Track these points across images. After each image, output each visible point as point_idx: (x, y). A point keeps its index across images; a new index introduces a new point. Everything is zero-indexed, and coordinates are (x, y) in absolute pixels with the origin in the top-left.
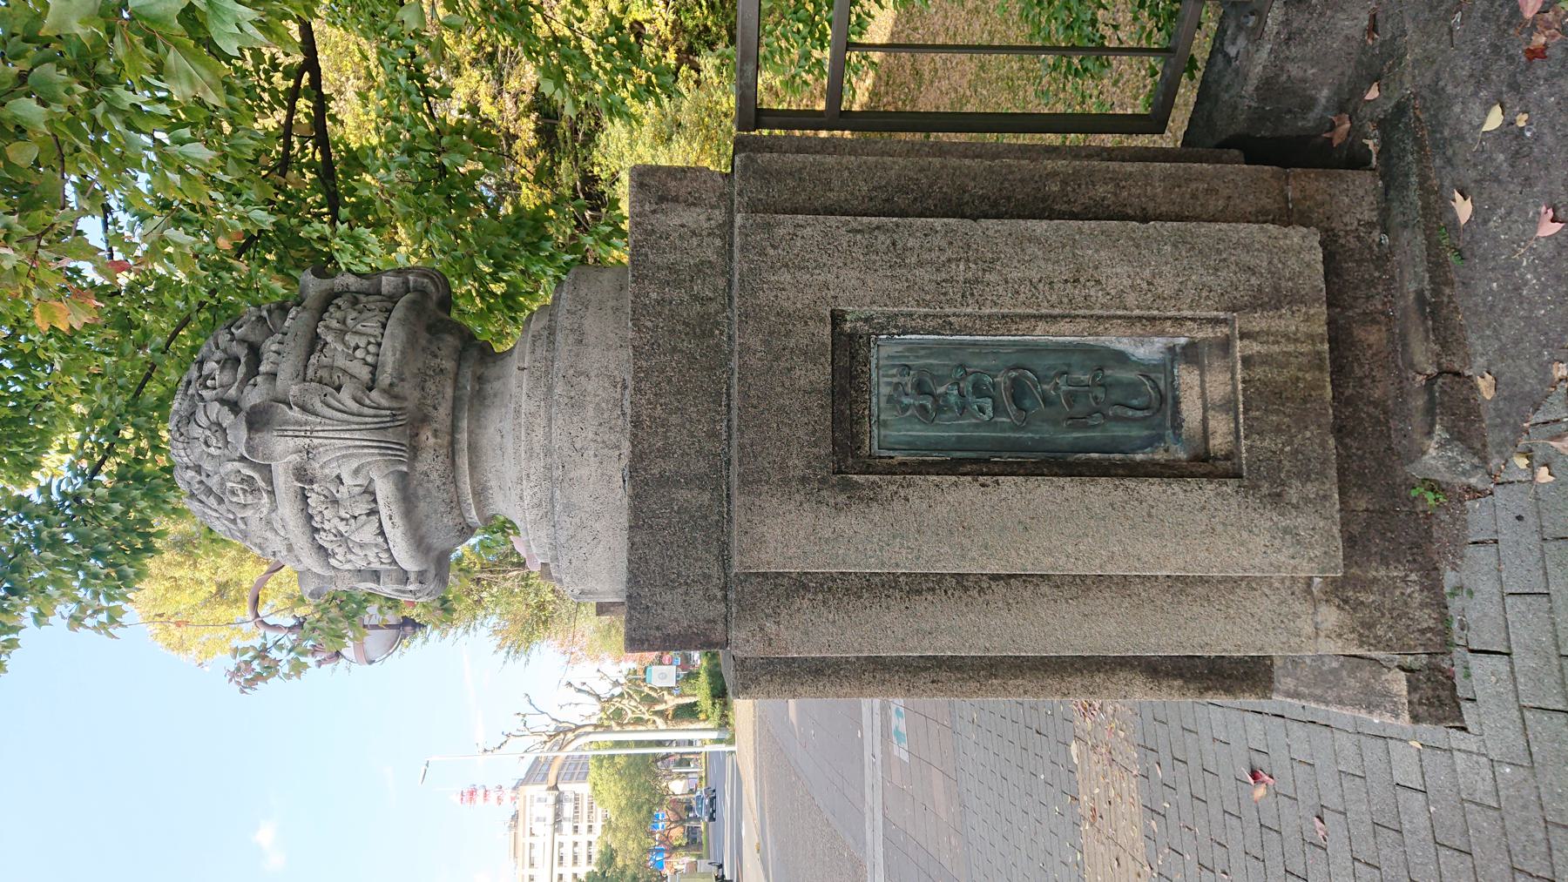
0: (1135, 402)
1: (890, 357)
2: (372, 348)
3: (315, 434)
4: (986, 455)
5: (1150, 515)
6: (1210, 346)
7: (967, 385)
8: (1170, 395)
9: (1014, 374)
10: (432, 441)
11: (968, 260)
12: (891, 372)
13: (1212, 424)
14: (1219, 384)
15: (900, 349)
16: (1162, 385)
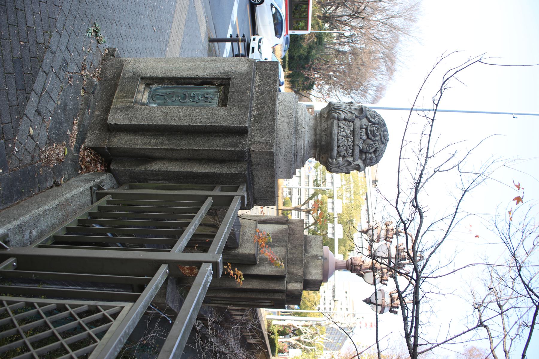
0: (158, 96)
2: (340, 131)
4: (195, 86)
6: (139, 104)
7: (196, 99)
8: (150, 97)
9: (185, 101)
10: (325, 115)
11: (192, 116)
13: (143, 90)
14: (140, 96)
16: (151, 99)
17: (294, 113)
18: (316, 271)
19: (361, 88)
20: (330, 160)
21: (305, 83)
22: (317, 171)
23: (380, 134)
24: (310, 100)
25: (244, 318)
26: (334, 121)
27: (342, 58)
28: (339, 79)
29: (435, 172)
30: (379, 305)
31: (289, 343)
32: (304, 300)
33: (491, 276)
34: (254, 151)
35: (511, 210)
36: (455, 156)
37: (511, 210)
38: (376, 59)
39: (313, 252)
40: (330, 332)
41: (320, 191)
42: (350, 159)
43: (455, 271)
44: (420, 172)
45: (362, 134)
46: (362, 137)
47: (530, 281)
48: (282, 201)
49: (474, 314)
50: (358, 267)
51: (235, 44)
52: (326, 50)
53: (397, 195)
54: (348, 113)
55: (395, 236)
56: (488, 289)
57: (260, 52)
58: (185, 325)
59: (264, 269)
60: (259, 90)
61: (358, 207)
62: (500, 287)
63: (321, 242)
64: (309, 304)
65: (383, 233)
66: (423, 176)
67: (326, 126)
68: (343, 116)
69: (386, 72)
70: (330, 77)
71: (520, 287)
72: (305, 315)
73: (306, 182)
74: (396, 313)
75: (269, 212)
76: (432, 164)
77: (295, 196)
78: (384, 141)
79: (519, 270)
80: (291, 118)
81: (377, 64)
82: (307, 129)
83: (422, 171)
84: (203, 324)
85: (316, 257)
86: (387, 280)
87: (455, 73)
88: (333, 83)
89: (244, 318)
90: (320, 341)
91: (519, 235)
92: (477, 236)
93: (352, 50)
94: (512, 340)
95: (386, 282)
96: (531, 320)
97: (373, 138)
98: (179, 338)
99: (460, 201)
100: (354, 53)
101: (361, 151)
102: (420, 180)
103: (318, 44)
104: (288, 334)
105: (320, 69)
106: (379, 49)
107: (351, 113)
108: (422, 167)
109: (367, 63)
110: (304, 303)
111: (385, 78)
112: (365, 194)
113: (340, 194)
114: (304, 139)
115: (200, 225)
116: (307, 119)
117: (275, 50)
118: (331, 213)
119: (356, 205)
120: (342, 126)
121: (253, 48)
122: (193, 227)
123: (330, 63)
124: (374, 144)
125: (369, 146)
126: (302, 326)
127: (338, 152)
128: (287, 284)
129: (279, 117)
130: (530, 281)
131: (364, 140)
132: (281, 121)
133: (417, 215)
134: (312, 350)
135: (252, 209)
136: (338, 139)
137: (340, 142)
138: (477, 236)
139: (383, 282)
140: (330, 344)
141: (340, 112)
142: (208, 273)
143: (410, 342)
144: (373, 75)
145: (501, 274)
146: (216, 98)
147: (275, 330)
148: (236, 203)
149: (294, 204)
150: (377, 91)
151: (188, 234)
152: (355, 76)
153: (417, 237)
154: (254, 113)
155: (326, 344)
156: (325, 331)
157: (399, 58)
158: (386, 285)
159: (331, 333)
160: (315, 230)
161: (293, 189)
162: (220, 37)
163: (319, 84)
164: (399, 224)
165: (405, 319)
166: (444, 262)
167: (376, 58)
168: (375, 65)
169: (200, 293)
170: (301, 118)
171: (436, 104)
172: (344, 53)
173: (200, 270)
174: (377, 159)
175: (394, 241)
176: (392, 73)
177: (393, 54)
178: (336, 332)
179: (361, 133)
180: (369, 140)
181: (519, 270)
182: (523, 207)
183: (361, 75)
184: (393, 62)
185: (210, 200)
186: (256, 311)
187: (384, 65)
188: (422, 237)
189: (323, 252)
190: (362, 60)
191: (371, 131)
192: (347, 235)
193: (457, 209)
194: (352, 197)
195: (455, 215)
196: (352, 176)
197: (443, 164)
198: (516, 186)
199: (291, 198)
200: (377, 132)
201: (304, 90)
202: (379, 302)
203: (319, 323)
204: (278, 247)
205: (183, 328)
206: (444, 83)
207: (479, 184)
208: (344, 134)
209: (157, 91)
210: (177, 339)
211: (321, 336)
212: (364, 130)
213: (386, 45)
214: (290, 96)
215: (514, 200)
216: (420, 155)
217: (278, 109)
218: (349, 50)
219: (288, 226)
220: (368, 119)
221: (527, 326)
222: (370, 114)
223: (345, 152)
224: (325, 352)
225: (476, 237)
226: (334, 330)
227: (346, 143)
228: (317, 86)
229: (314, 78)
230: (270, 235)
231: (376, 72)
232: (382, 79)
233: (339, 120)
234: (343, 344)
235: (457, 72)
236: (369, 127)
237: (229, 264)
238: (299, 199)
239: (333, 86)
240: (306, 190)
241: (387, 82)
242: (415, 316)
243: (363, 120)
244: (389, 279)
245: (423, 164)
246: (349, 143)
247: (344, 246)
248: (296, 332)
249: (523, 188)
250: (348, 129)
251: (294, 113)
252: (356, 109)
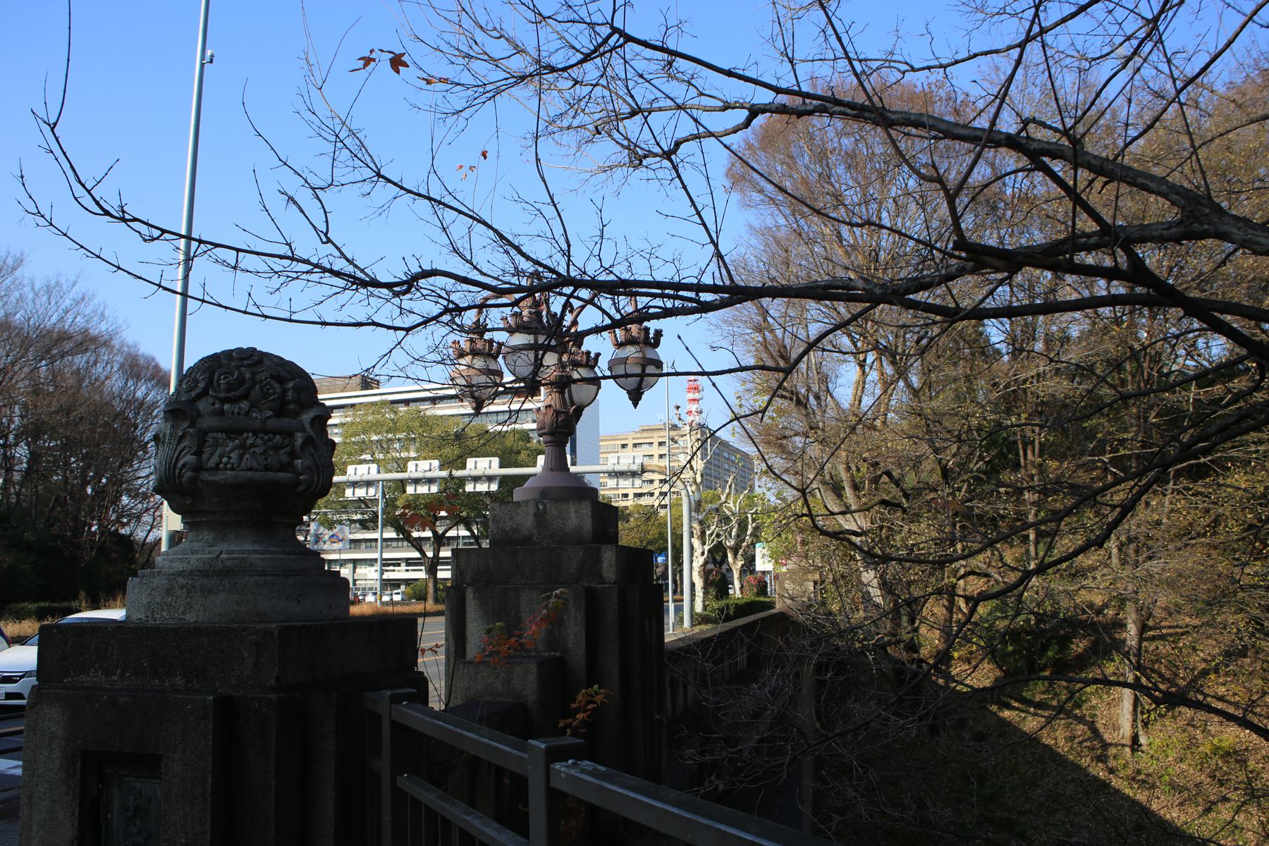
2: (229, 466)
17: (181, 581)
18: (573, 515)
19: (131, 415)
20: (301, 488)
21: (114, 555)
22: (340, 522)
23: (238, 368)
24: (158, 542)
25: (691, 678)
26: (202, 481)
27: (48, 462)
28: (106, 471)
29: (329, 241)
30: (644, 370)
31: (743, 572)
32: (644, 544)
33: (569, 128)
34: (277, 678)
35: (424, 79)
36: (291, 194)
37: (424, 79)
38: (54, 377)
39: (529, 523)
40: (713, 479)
41: (388, 513)
42: (299, 439)
43: (553, 202)
44: (327, 274)
45: (236, 410)
46: (243, 412)
47: (578, 51)
48: (416, 603)
49: (653, 167)
50: (560, 419)
52: (24, 505)
53: (333, 321)
54: (182, 445)
55: (487, 336)
56: (598, 136)
57: (21, 677)
58: (694, 817)
59: (571, 639)
60: (118, 671)
61: (426, 422)
62: (592, 111)
63: (503, 506)
64: (653, 532)
65: (479, 363)
66: (336, 268)
67: (216, 499)
68: (189, 458)
69: (89, 354)
70: (100, 493)
71: (591, 71)
72: (678, 538)
73: (366, 547)
74: (659, 334)
75: (433, 633)
76: (308, 246)
77: (400, 573)
78: (250, 359)
79: (553, 69)
80: (194, 587)
81: (68, 375)
82: (223, 547)
83: (324, 270)
84: (710, 775)
85: (540, 517)
86: (588, 353)
87: (83, 186)
88: (115, 484)
89: (691, 678)
90: (735, 503)
91: (478, 66)
92: (484, 155)
93: (27, 439)
94: (702, 94)
95: (592, 355)
96: (659, 55)
97: (246, 386)
98: (723, 827)
99: (402, 188)
100: (33, 432)
101: (280, 412)
102: (345, 275)
103: (7, 526)
104: (723, 576)
105: (76, 519)
106: (26, 370)
107: (182, 438)
108: (316, 270)
109: (63, 400)
110: (650, 542)
111: (106, 358)
112: (396, 405)
113: (395, 465)
114: (249, 552)
115: (472, 804)
116: (196, 546)
117: (19, 637)
118: (440, 485)
119: (421, 426)
120: (215, 459)
121: (9, 696)
122: (469, 818)
123: (62, 494)
124: (261, 381)
125: (265, 395)
126: (704, 544)
127: (282, 468)
128: (604, 583)
129: (190, 617)
130: (578, 51)
131: (252, 406)
132: (201, 613)
133: (422, 282)
134: (754, 520)
135: (426, 675)
136: (247, 470)
137: (255, 464)
138: (484, 155)
139: (592, 363)
140: (740, 479)
141: (179, 465)
142: (572, 772)
143: (718, 302)
144: (97, 385)
145: (564, 106)
146: (138, 785)
147: (716, 606)
148: (409, 714)
149: (421, 574)
150: (138, 378)
151: (488, 830)
152: (99, 430)
153: (484, 286)
154: (179, 681)
155: (740, 489)
156: (711, 491)
157: (54, 319)
158: (598, 355)
159: (716, 478)
160: (482, 523)
161: (385, 576)
163: (118, 520)
164: (458, 325)
165: (667, 313)
166: (540, 225)
167: (50, 377)
168: (71, 382)
169: (620, 786)
170: (194, 561)
171: (160, 232)
172: (34, 457)
173: (568, 791)
174: (299, 377)
175: (501, 337)
176: (94, 339)
177: (41, 336)
178: (713, 467)
179: (233, 413)
180: (253, 393)
181: (553, 69)
182: (415, 53)
183: (97, 417)
184: (64, 336)
185: (404, 780)
186: (672, 652)
187: (70, 358)
188: (485, 275)
189: (527, 502)
190: (55, 412)
191: (228, 391)
192: (487, 444)
193: (419, 195)
194: (401, 436)
195: (435, 201)
196: (352, 436)
197: (311, 223)
198: (365, 66)
199: (407, 582)
200: (233, 375)
201: (134, 556)
202: (638, 370)
203: (693, 506)
204: (519, 607)
205: (701, 820)
206: (107, 213)
207: (363, 146)
208: (234, 455)
210: (725, 833)
211: (723, 498)
212: (226, 407)
213: (15, 353)
214: (136, 590)
215: (398, 72)
216: (290, 274)
217: (169, 622)
218: (26, 445)
219: (468, 585)
220: (199, 397)
221: (670, 63)
222: (186, 392)
223: (282, 452)
224: (758, 491)
225: (485, 158)
226: (708, 472)
227: (259, 450)
228: (124, 525)
229: (102, 534)
230: (486, 627)
231: (90, 378)
232: (107, 363)
233: (198, 468)
234: (738, 451)
235: (80, 182)
236: (219, 395)
237: (561, 724)
238: (409, 562)
239: (124, 486)
240: (388, 546)
241: (116, 352)
242: (660, 291)
243: (201, 408)
244: (584, 348)
245: (308, 267)
246: (259, 441)
247: (519, 453)
248: (718, 558)
249: (372, 51)
250: (223, 445)
251: (181, 581)
252: (173, 426)
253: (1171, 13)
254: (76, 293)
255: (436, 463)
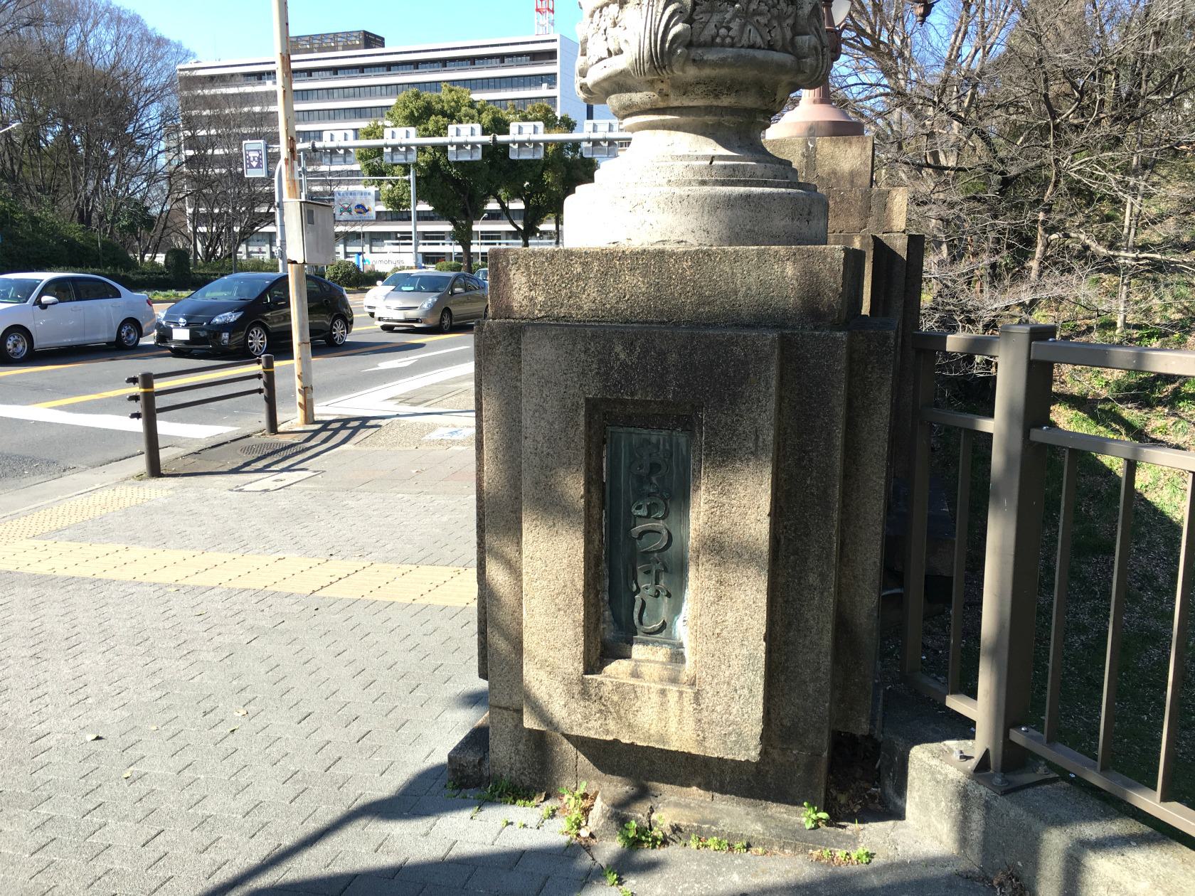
1: (678, 444)
2: (728, 40)
3: (650, 8)
5: (559, 610)
12: (667, 445)
15: (684, 453)
51: (160, 402)
137: (759, 40)
141: (670, 37)
162: (142, 446)
208: (735, 25)
209: (624, 619)
227: (763, 20)
253: (403, 396)
254: (667, 189)
255: (478, 127)
